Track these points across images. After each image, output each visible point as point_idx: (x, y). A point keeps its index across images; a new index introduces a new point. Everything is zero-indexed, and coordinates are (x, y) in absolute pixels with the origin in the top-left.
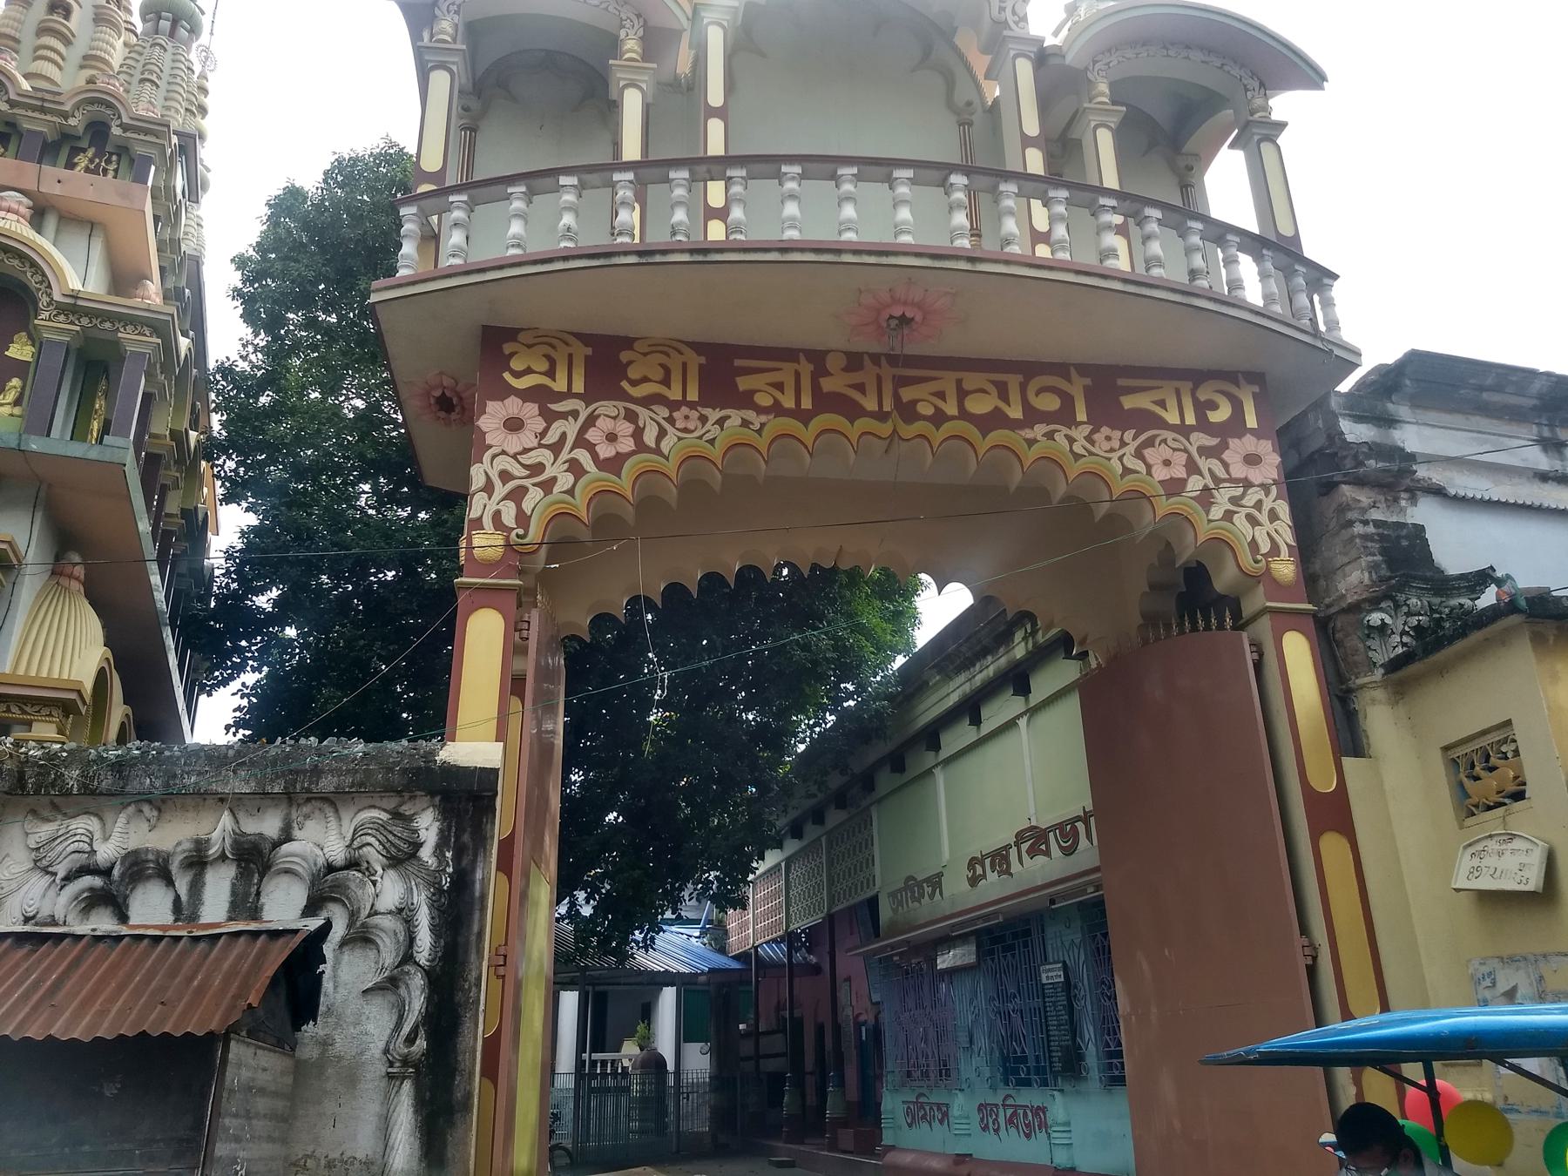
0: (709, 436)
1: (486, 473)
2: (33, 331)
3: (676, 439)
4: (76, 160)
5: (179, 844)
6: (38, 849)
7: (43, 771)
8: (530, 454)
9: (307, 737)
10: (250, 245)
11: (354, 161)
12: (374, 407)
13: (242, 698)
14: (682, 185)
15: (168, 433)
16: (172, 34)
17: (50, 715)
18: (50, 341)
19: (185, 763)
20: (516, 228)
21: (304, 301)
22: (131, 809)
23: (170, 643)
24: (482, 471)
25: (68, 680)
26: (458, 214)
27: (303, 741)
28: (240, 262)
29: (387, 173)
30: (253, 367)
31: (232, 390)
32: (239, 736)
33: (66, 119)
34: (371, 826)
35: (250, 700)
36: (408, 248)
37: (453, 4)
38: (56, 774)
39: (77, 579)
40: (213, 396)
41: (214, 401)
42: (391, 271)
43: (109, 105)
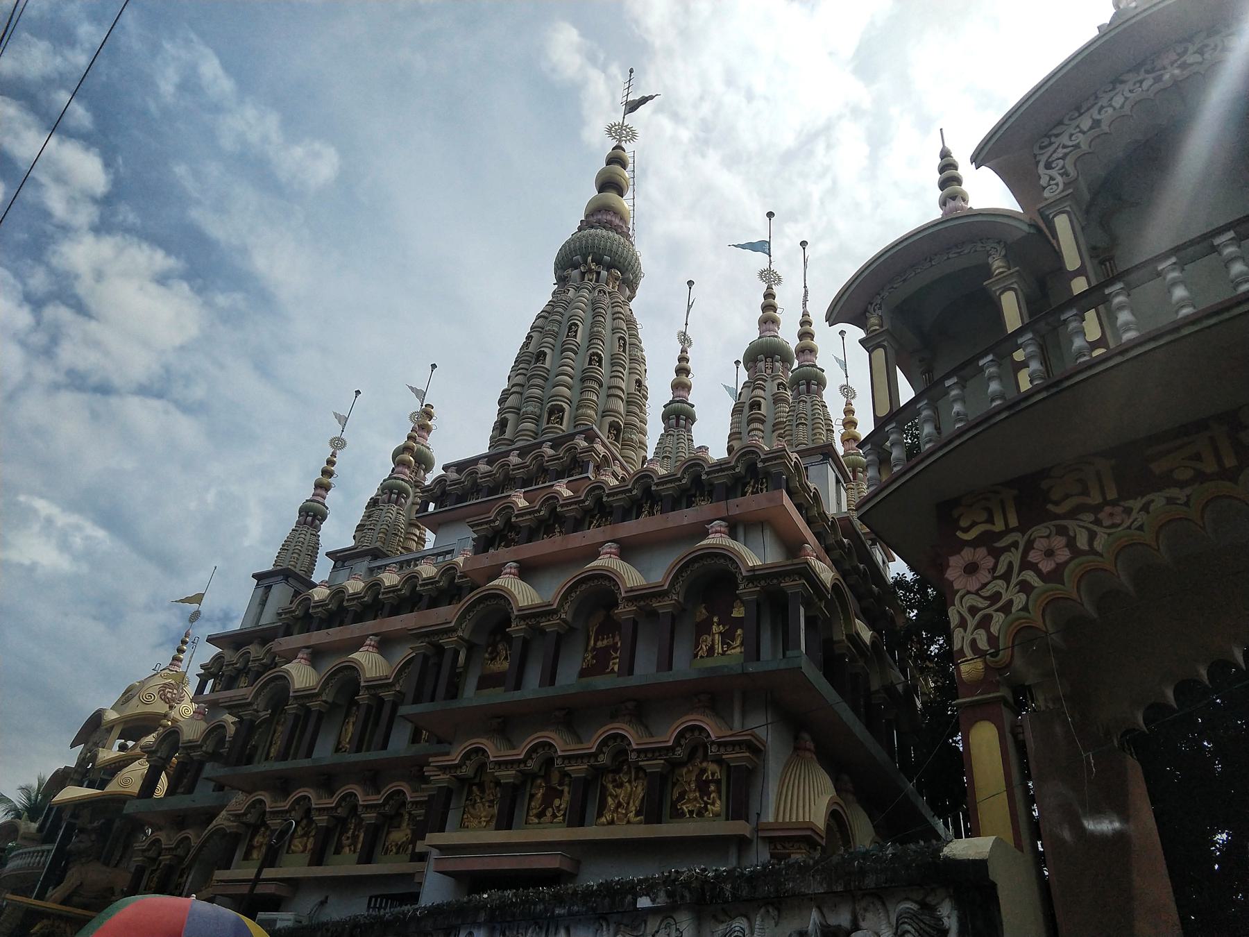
0: (1136, 524)
1: (959, 612)
3: (1106, 536)
8: (988, 587)
14: (1030, 344)
15: (844, 638)
17: (800, 848)
19: (786, 873)
22: (762, 910)
24: (955, 611)
34: (906, 915)
39: (809, 750)
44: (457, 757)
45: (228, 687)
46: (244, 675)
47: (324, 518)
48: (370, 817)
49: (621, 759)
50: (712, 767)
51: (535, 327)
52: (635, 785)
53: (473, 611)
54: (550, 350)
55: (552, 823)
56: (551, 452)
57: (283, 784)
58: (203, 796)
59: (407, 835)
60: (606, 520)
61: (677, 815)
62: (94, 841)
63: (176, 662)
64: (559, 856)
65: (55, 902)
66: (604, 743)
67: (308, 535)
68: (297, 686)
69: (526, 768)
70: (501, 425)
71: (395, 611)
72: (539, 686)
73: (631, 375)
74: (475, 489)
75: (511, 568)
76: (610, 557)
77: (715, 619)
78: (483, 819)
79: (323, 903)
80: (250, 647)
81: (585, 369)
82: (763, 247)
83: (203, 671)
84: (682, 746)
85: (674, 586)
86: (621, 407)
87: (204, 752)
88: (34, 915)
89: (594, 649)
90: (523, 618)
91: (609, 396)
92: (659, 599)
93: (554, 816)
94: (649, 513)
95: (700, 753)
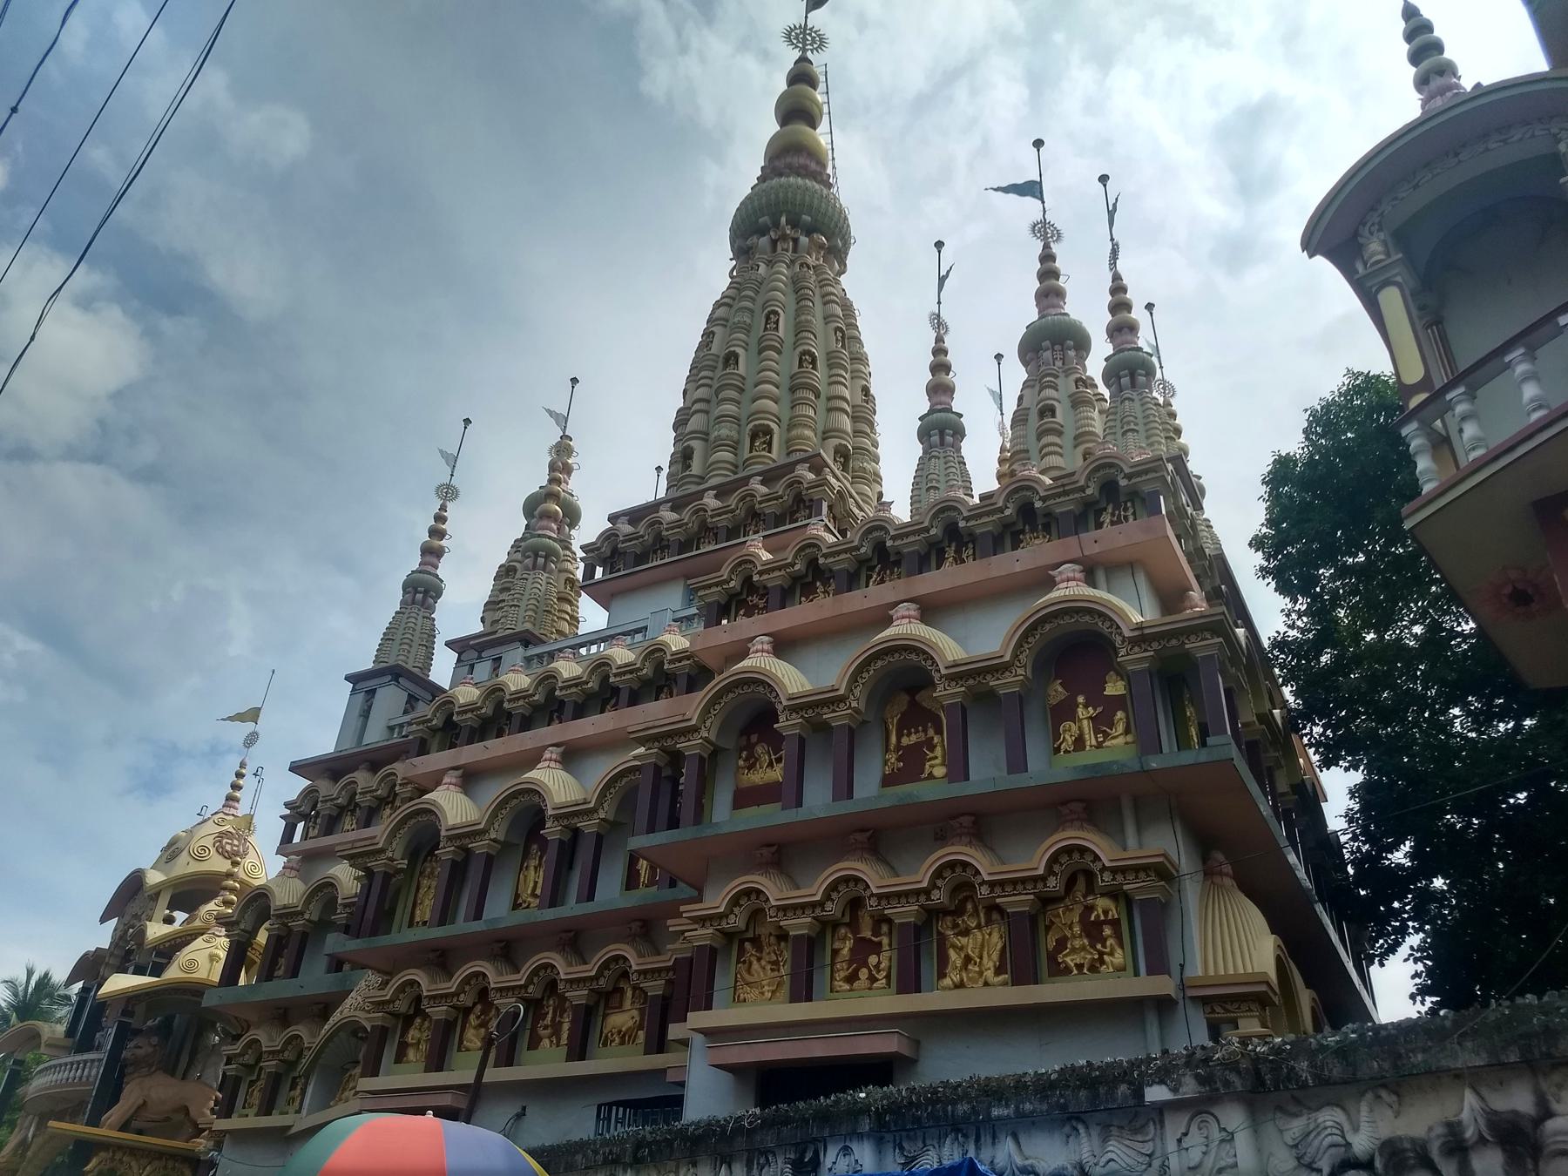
2: (1117, 667)
4: (1102, 520)
5: (1430, 1129)
6: (1296, 1146)
7: (1275, 1067)
9: (1522, 995)
10: (1262, 525)
11: (1327, 407)
12: (1434, 628)
13: (1415, 963)
15: (1255, 718)
16: (1133, 385)
17: (1251, 1011)
18: (1134, 672)
19: (1405, 1040)
20: (1530, 391)
21: (1329, 554)
22: (1369, 1096)
23: (1326, 920)
25: (1246, 974)
26: (1460, 409)
27: (1519, 1000)
28: (1257, 543)
29: (1361, 403)
30: (1302, 631)
31: (1292, 660)
32: (1428, 1004)
33: (1084, 492)
35: (1425, 965)
36: (1423, 463)
37: (1373, 225)
38: (1287, 1068)
39: (1227, 875)
40: (1277, 671)
41: (1280, 676)
42: (1416, 491)
43: (1111, 465)
44: (721, 903)
45: (328, 831)
46: (349, 813)
47: (439, 594)
48: (578, 996)
49: (961, 897)
50: (1102, 903)
51: (717, 319)
52: (988, 932)
53: (720, 703)
54: (743, 350)
55: (870, 989)
56: (764, 490)
57: (441, 958)
58: (314, 979)
59: (633, 1018)
60: (892, 573)
61: (1059, 971)
62: (155, 1046)
63: (231, 803)
64: (896, 1035)
65: (111, 1128)
66: (834, 887)
67: (420, 618)
68: (451, 822)
69: (825, 913)
70: (683, 457)
71: (580, 711)
72: (833, 801)
73: (856, 380)
74: (660, 544)
75: (762, 643)
76: (910, 622)
77: (1081, 699)
78: (766, 988)
79: (521, 1115)
80: (395, 765)
81: (795, 375)
82: (1032, 189)
83: (288, 812)
84: (1055, 875)
85: (1017, 656)
86: (847, 424)
87: (307, 920)
88: (84, 1149)
89: (899, 747)
90: (794, 709)
91: (829, 410)
92: (996, 676)
93: (873, 979)
94: (955, 559)
95: (1081, 884)
